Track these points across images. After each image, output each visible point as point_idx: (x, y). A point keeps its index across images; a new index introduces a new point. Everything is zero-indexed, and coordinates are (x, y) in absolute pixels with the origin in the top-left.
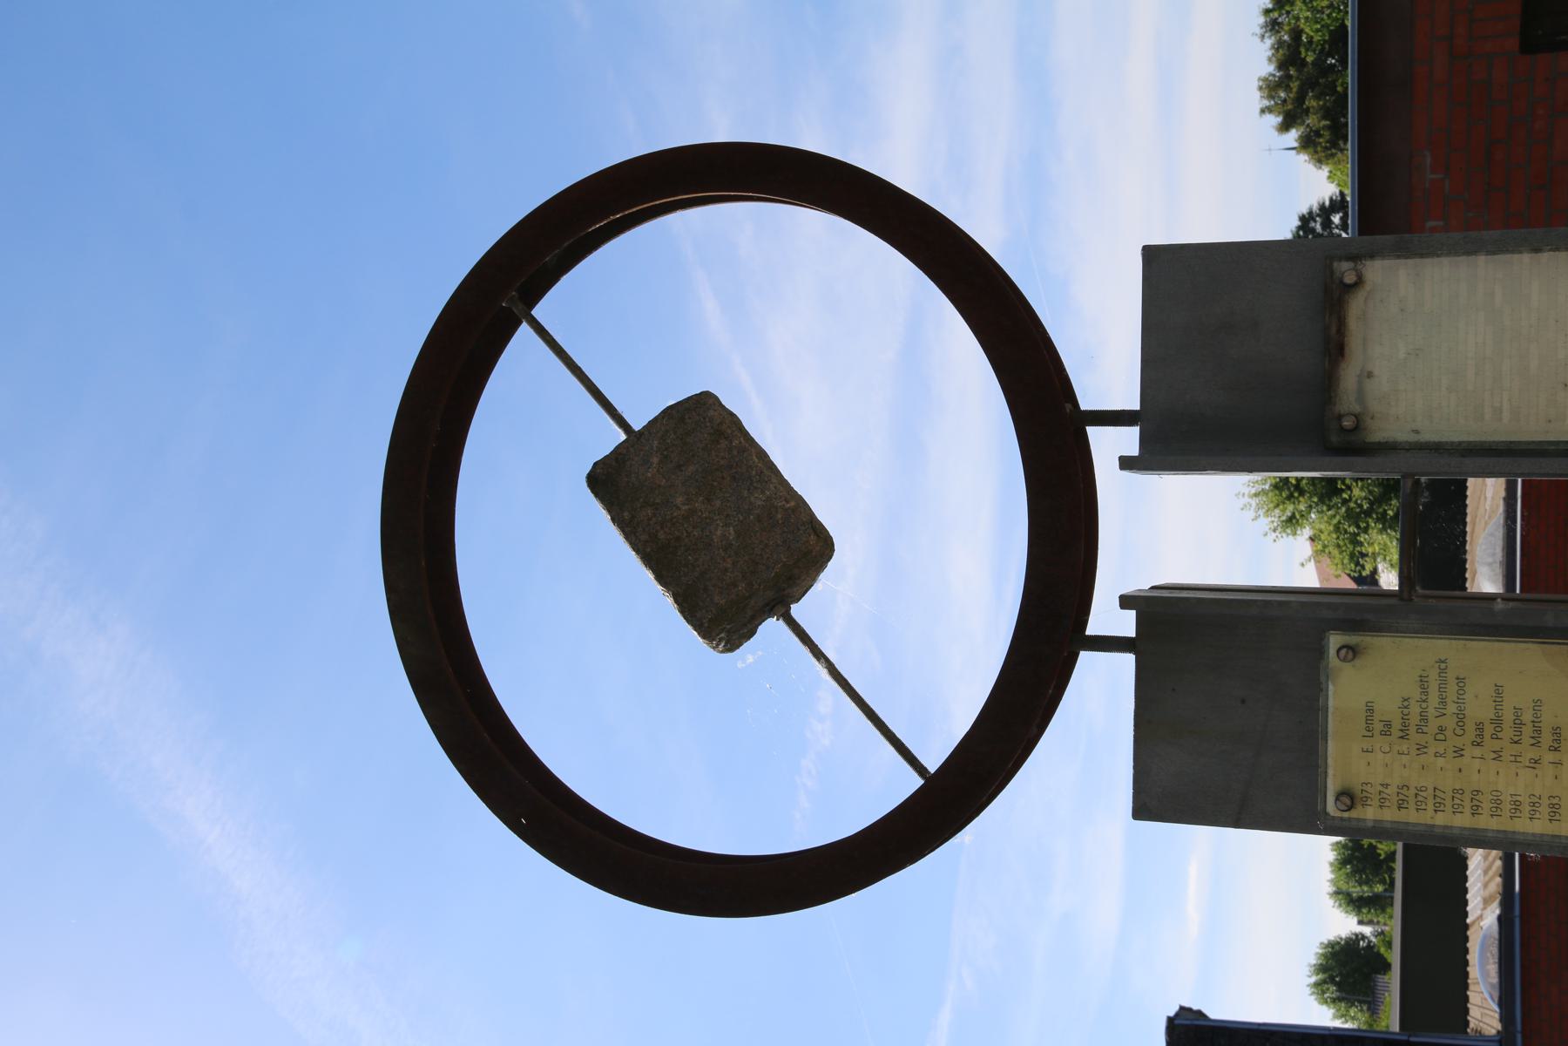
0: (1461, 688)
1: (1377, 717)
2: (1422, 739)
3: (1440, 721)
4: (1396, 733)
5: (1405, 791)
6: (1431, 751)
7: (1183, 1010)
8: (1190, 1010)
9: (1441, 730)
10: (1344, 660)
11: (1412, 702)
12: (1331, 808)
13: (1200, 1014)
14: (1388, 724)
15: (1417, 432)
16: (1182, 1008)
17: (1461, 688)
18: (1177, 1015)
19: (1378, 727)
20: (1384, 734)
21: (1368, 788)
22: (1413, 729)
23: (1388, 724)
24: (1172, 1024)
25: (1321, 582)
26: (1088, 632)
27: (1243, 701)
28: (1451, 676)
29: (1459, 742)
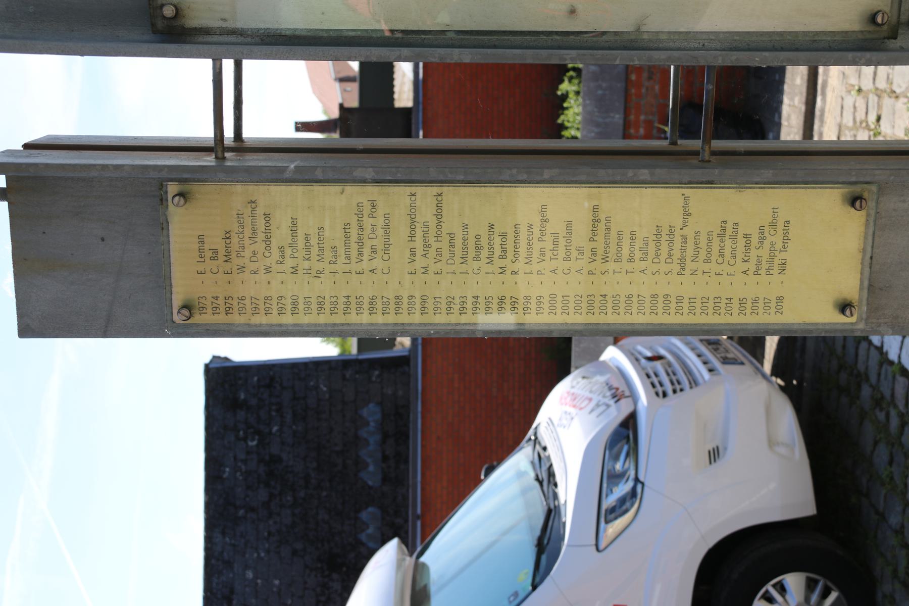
0: (267, 222)
1: (207, 247)
2: (240, 262)
3: (252, 248)
4: (222, 258)
5: (230, 301)
6: (247, 271)
7: (215, 358)
8: (219, 357)
9: (254, 253)
10: (177, 205)
11: (233, 234)
12: (177, 318)
13: (226, 359)
14: (215, 252)
15: (225, 20)
16: (214, 357)
17: (267, 222)
18: (211, 361)
19: (209, 254)
20: (213, 259)
21: (202, 300)
22: (234, 255)
23: (215, 252)
24: (208, 369)
25: (325, 112)
26: (5, 186)
27: (103, 240)
28: (260, 211)
29: (268, 262)
